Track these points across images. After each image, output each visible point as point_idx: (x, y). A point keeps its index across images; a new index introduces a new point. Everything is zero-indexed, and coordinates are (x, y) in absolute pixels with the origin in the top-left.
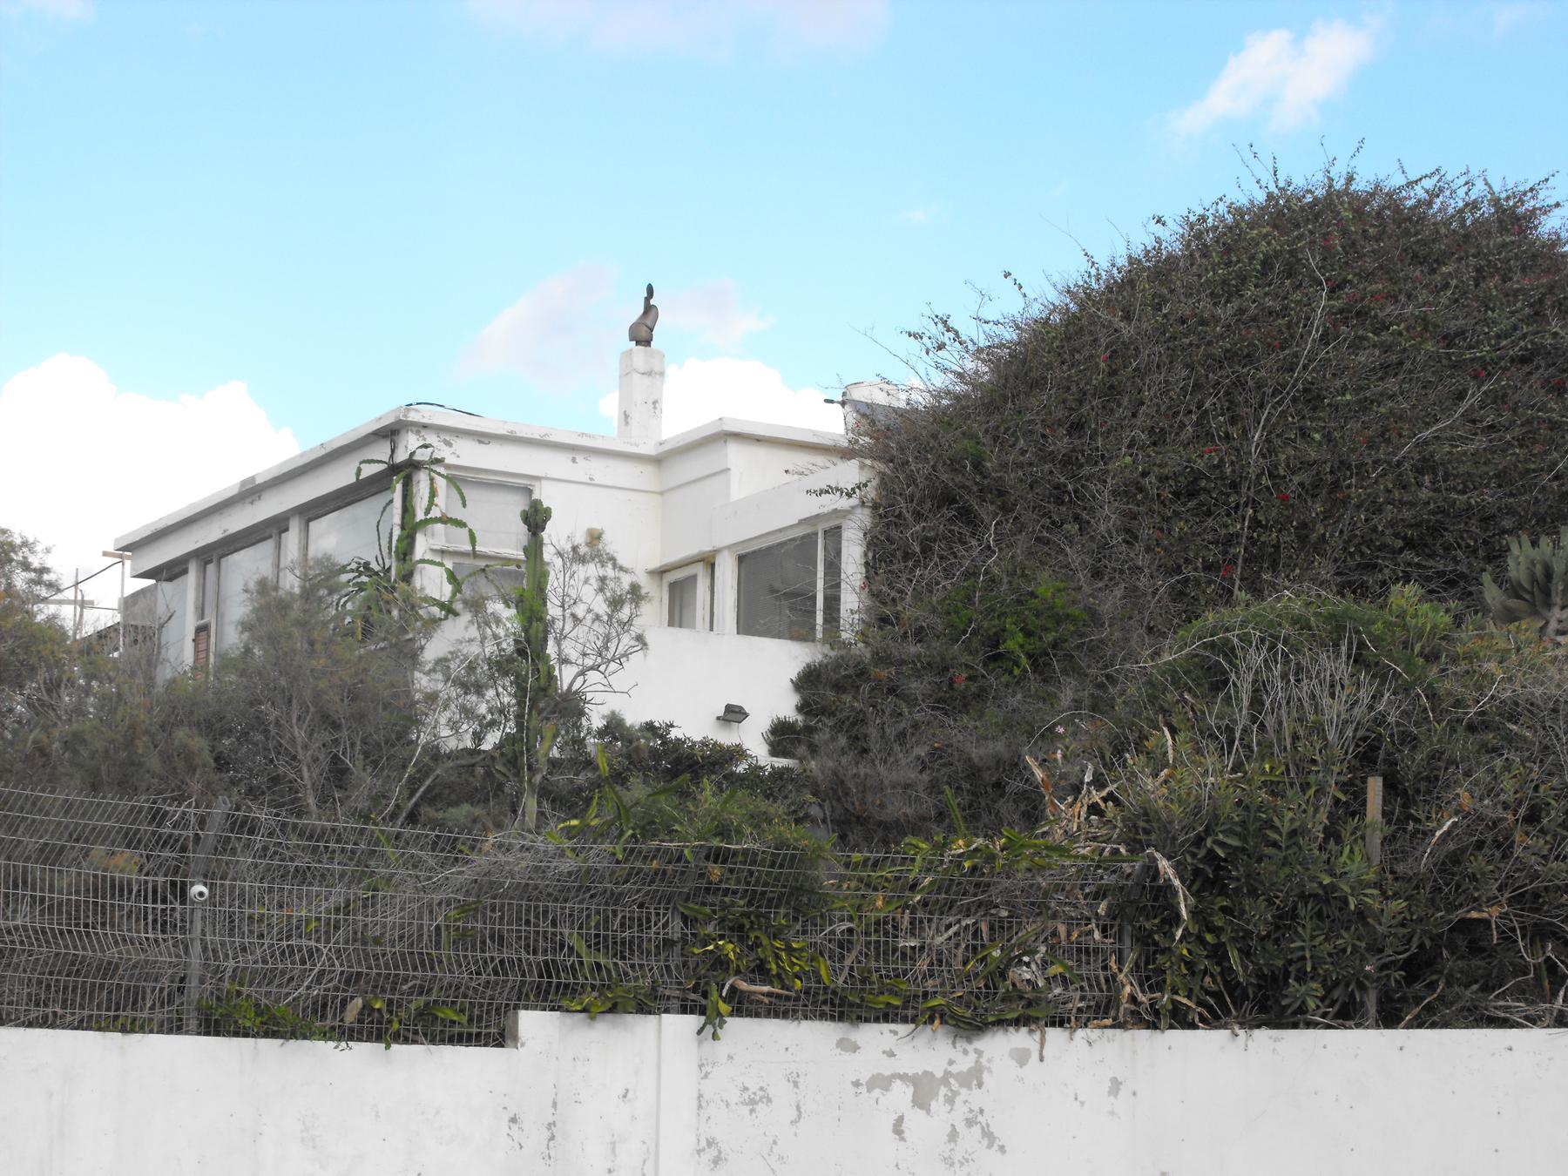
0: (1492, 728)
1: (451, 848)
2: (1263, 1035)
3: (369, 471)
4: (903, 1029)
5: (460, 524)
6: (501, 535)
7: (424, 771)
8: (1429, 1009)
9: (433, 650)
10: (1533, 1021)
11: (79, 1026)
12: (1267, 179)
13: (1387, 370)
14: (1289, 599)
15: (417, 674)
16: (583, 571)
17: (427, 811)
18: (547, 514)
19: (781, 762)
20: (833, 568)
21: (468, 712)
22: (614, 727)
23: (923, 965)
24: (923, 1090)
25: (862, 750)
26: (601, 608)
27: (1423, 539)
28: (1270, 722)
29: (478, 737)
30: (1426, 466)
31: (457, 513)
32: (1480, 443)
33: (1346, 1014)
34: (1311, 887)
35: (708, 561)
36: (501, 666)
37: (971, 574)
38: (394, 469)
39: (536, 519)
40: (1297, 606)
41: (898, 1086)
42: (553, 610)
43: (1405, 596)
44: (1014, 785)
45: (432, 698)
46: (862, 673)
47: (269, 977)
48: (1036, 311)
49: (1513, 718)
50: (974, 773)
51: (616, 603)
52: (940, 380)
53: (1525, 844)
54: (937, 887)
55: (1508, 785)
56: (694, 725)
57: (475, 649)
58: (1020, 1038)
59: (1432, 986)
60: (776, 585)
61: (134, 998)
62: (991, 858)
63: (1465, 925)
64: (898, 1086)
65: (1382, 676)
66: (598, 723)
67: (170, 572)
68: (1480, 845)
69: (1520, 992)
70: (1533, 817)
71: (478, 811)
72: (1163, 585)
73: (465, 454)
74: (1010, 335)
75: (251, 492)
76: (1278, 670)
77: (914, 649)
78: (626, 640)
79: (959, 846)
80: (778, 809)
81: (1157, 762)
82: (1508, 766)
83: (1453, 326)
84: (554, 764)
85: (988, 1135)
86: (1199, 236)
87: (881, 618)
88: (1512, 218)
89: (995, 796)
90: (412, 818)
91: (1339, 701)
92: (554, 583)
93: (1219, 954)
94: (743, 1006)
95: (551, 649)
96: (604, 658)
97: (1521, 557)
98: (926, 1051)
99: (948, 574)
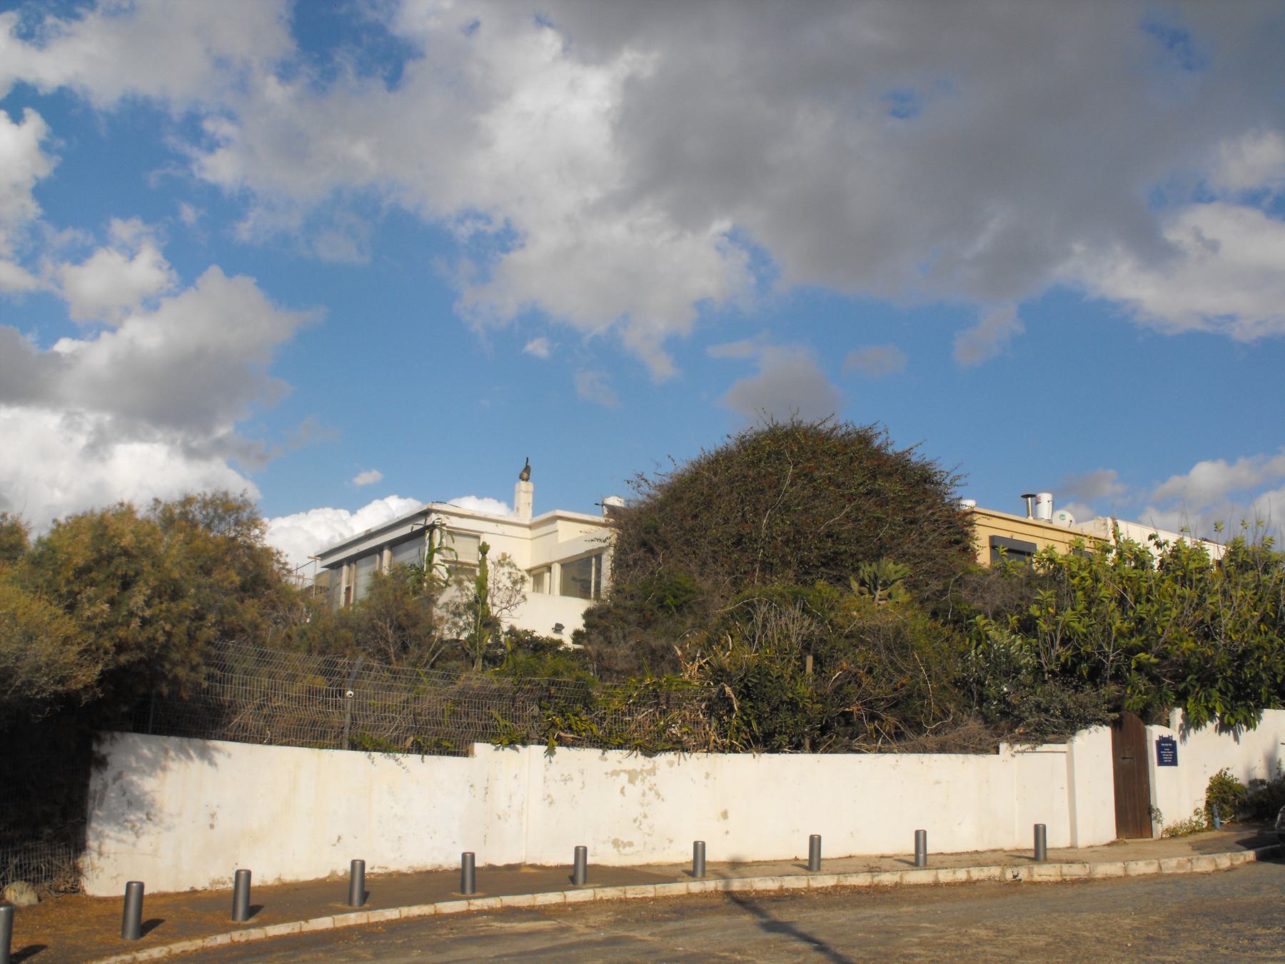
0: (855, 638)
1: (449, 677)
2: (766, 756)
3: (416, 528)
4: (625, 752)
5: (452, 550)
6: (467, 553)
7: (437, 648)
8: (830, 746)
9: (443, 599)
10: (869, 751)
11: (302, 746)
12: (769, 421)
13: (815, 497)
14: (777, 586)
15: (435, 609)
16: (502, 570)
17: (439, 664)
18: (488, 547)
19: (577, 646)
20: (599, 571)
21: (455, 624)
22: (512, 631)
23: (633, 727)
24: (632, 776)
25: (609, 642)
26: (509, 585)
27: (831, 561)
28: (770, 634)
29: (458, 634)
30: (829, 535)
31: (451, 546)
32: (850, 526)
33: (797, 747)
34: (785, 698)
35: (549, 567)
36: (469, 606)
37: (652, 573)
38: (426, 528)
39: (484, 549)
40: (780, 589)
41: (622, 775)
42: (490, 585)
43: (821, 584)
44: (669, 657)
45: (441, 619)
46: (609, 611)
47: (376, 728)
48: (679, 471)
49: (862, 633)
50: (653, 652)
51: (515, 583)
52: (640, 498)
53: (866, 681)
54: (639, 696)
55: (860, 659)
56: (544, 631)
57: (458, 600)
58: (670, 756)
59: (831, 737)
60: (577, 574)
61: (323, 735)
62: (661, 686)
63: (844, 714)
64: (622, 775)
65: (813, 617)
66: (506, 629)
67: (337, 566)
68: (849, 683)
69: (865, 740)
70: (870, 671)
71: (459, 663)
72: (728, 580)
73: (454, 522)
74: (668, 480)
75: (369, 536)
76: (773, 613)
77: (629, 603)
78: (519, 597)
79: (648, 681)
80: (576, 664)
81: (724, 648)
82: (861, 652)
83: (841, 480)
84: (489, 646)
85: (658, 794)
86: (742, 443)
87: (617, 590)
88: (864, 439)
89: (658, 658)
90: (433, 666)
91: (796, 625)
92: (490, 575)
93: (748, 724)
94: (562, 742)
95: (489, 600)
96: (510, 604)
97: (866, 570)
98: (637, 761)
99: (644, 573)
